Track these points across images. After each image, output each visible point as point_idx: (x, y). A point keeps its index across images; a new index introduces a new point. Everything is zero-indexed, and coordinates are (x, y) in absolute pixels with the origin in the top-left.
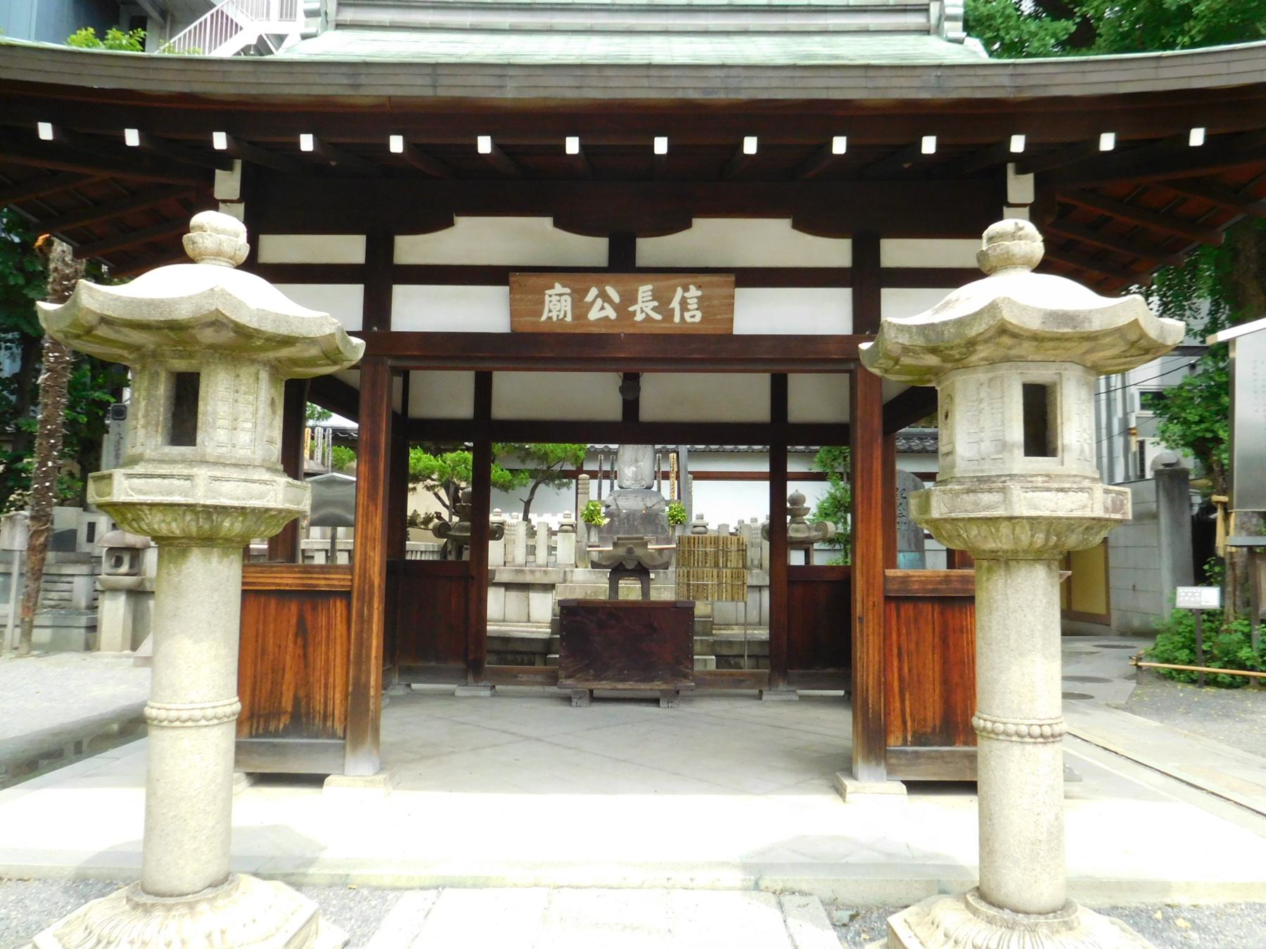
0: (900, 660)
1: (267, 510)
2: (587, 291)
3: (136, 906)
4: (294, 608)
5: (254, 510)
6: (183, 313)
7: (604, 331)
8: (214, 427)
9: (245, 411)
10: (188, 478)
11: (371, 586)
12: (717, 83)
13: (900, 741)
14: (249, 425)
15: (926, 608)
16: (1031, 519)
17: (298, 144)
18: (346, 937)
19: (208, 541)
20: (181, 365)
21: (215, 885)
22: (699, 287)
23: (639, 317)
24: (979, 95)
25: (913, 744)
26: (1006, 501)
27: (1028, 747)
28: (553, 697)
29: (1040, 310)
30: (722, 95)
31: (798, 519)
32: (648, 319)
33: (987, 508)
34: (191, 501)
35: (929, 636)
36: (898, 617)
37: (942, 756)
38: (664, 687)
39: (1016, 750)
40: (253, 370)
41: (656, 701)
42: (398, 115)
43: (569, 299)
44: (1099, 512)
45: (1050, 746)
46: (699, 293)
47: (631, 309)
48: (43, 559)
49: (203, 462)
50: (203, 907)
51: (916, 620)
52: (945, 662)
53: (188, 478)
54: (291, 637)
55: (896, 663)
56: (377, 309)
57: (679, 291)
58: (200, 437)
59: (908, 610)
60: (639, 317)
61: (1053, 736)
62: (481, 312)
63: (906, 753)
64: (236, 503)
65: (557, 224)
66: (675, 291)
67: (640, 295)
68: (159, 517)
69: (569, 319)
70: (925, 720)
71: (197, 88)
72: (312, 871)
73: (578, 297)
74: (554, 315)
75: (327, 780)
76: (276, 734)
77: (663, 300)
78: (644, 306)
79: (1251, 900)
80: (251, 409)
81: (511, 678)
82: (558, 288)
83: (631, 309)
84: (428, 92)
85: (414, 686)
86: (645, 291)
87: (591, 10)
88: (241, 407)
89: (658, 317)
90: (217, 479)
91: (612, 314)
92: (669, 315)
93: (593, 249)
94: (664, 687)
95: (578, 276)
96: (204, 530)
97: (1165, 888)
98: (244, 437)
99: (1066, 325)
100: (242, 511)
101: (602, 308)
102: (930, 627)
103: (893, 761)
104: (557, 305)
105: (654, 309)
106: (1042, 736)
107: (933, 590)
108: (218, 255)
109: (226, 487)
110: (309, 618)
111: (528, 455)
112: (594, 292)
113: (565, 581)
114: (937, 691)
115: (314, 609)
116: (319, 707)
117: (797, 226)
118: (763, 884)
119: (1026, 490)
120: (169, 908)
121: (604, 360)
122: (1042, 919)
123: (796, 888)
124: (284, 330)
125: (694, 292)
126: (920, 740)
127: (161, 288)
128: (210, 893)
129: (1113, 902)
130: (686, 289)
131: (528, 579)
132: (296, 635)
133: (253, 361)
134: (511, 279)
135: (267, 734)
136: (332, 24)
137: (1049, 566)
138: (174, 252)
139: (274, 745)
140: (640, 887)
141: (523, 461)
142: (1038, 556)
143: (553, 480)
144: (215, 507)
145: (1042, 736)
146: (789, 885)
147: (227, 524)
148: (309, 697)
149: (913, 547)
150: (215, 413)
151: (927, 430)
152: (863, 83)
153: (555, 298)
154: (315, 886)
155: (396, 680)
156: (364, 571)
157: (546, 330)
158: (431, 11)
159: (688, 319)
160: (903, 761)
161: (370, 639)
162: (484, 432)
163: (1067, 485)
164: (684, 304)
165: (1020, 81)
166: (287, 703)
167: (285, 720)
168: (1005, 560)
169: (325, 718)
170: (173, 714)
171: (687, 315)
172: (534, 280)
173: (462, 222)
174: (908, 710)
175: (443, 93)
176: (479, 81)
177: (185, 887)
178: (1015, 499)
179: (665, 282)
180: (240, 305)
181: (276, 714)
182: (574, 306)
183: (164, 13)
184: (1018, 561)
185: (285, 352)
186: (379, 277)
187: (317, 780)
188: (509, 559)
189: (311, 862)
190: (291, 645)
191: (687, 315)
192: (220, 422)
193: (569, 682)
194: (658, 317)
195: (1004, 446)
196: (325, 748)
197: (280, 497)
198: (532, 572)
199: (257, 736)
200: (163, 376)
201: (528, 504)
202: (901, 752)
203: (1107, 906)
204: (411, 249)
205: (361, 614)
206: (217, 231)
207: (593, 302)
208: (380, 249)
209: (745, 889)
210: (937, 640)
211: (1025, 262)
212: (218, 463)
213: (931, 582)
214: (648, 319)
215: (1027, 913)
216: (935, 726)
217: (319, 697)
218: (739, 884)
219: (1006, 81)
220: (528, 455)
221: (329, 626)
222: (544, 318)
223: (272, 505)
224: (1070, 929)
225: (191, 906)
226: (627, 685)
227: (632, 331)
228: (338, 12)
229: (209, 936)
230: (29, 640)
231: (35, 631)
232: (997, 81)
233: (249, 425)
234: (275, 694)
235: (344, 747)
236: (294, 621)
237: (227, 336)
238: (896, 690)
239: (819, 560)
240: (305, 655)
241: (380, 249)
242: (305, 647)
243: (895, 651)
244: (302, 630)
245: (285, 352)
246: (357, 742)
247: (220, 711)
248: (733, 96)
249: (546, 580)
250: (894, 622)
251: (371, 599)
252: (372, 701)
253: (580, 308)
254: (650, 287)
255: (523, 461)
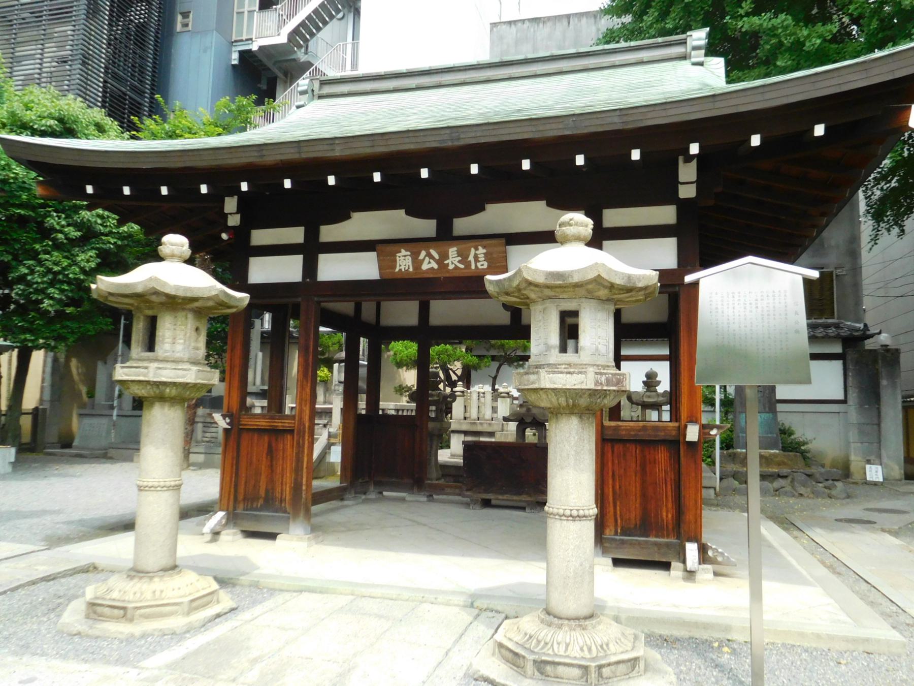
0: (614, 480)
1: (188, 384)
2: (419, 253)
3: (128, 576)
4: (266, 438)
5: (180, 383)
6: (139, 290)
7: (431, 276)
8: (163, 343)
9: (180, 334)
10: (146, 368)
11: (304, 425)
12: (446, 137)
13: (613, 532)
14: (182, 341)
15: (632, 447)
16: (554, 390)
17: (240, 187)
18: (234, 606)
19: (162, 399)
20: (150, 313)
21: (165, 570)
22: (484, 247)
23: (451, 267)
24: (600, 129)
25: (622, 535)
26: (539, 379)
27: (565, 522)
28: (462, 503)
29: (543, 272)
30: (450, 144)
31: (652, 389)
32: (456, 268)
33: (533, 383)
34: (147, 379)
35: (633, 465)
36: (613, 451)
37: (639, 543)
38: (529, 499)
39: (558, 523)
40: (184, 313)
41: (523, 509)
42: (287, 168)
43: (410, 258)
44: (591, 385)
45: (577, 523)
46: (485, 251)
47: (446, 262)
48: (195, 413)
49: (156, 360)
50: (156, 579)
51: (624, 455)
52: (643, 482)
53: (146, 368)
54: (264, 455)
55: (611, 482)
56: (310, 268)
57: (473, 250)
58: (157, 348)
59: (619, 448)
60: (451, 267)
61: (584, 516)
62: (362, 268)
63: (616, 540)
64: (169, 380)
65: (407, 213)
66: (470, 250)
67: (450, 254)
68: (137, 387)
69: (411, 270)
70: (629, 519)
71: (189, 164)
72: (242, 578)
73: (415, 256)
74: (403, 268)
75: (279, 536)
76: (256, 509)
77: (464, 259)
78: (453, 260)
79: (787, 642)
80: (183, 333)
81: (440, 490)
82: (403, 252)
83: (446, 262)
84: (296, 156)
85: (385, 493)
86: (453, 251)
87: (465, 70)
88: (178, 332)
89: (462, 266)
90: (160, 368)
91: (436, 266)
92: (468, 265)
93: (427, 227)
94: (529, 499)
95: (413, 244)
96: (162, 393)
97: (727, 629)
98: (179, 348)
99: (559, 280)
100: (174, 384)
101: (429, 263)
102: (634, 460)
103: (607, 545)
104: (404, 262)
105: (459, 262)
106: (578, 516)
107: (635, 435)
108: (173, 256)
109: (164, 372)
110: (274, 445)
111: (493, 346)
112: (423, 253)
113: (503, 430)
114: (638, 501)
115: (277, 440)
116: (278, 495)
117: (549, 205)
118: (476, 604)
119: (549, 372)
120: (141, 578)
121: (440, 293)
122: (566, 622)
123: (495, 608)
124: (189, 295)
125: (481, 250)
126: (625, 532)
127: (140, 277)
128: (161, 573)
129: (691, 634)
130: (477, 249)
131: (479, 428)
132: (267, 455)
133: (184, 309)
134: (377, 248)
135: (252, 509)
136: (316, 97)
137: (580, 417)
138: (156, 257)
139: (255, 516)
140: (407, 600)
141: (488, 350)
142: (173, 401)
143: (513, 362)
144: (160, 382)
145: (571, 516)
146: (491, 606)
147: (168, 390)
148: (273, 489)
149: (767, 409)
150: (164, 336)
151: (830, 321)
152: (530, 129)
153: (402, 258)
154: (242, 586)
155: (372, 488)
156: (301, 418)
157: (399, 277)
158: (372, 82)
159: (480, 267)
160: (614, 545)
161: (303, 456)
162: (426, 334)
163: (572, 370)
164: (476, 259)
165: (625, 119)
166: (262, 493)
167: (261, 502)
168: (557, 412)
169: (281, 501)
170: (145, 484)
171: (479, 265)
172: (390, 248)
173: (357, 216)
174: (618, 512)
175: (304, 156)
176: (321, 148)
177: (149, 569)
178: (542, 378)
179: (464, 245)
180: (165, 284)
181: (255, 498)
182: (413, 262)
183: (286, 74)
184: (562, 414)
185: (196, 304)
186: (311, 250)
187: (272, 536)
188: (481, 416)
189: (244, 574)
190: (264, 459)
191: (479, 265)
192: (167, 340)
193: (469, 493)
194: (462, 266)
195: (548, 348)
196: (280, 518)
197: (193, 377)
198: (481, 424)
199: (247, 510)
200: (142, 317)
201: (495, 379)
202: (613, 539)
203: (687, 637)
204: (329, 233)
205: (298, 443)
206: (172, 245)
207: (424, 259)
208: (312, 234)
209: (465, 606)
210: (638, 468)
211: (577, 238)
212: (165, 360)
213: (634, 430)
214: (456, 268)
215: (555, 617)
216: (636, 525)
217: (278, 490)
218: (462, 603)
219: (616, 120)
220: (493, 346)
221: (284, 450)
222: (397, 270)
223: (189, 381)
224: (584, 629)
225: (151, 578)
226: (505, 497)
227: (447, 275)
228: (320, 90)
229: (154, 592)
230: (188, 460)
231: (191, 455)
232: (609, 120)
233: (182, 341)
234: (256, 486)
235: (289, 518)
236: (266, 445)
237: (163, 299)
238: (611, 499)
239: (405, 414)
240: (272, 466)
241: (312, 234)
242: (271, 461)
243: (611, 474)
244: (271, 452)
245: (196, 304)
246: (296, 515)
247: (168, 484)
248: (456, 143)
249: (490, 430)
250: (610, 455)
251: (304, 432)
252: (304, 493)
253: (417, 263)
254: (455, 249)
255: (488, 350)
